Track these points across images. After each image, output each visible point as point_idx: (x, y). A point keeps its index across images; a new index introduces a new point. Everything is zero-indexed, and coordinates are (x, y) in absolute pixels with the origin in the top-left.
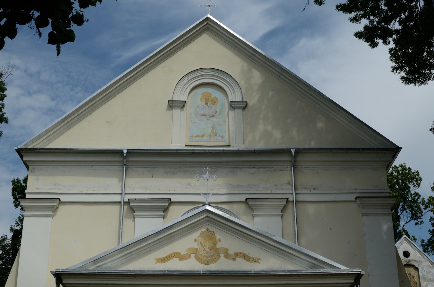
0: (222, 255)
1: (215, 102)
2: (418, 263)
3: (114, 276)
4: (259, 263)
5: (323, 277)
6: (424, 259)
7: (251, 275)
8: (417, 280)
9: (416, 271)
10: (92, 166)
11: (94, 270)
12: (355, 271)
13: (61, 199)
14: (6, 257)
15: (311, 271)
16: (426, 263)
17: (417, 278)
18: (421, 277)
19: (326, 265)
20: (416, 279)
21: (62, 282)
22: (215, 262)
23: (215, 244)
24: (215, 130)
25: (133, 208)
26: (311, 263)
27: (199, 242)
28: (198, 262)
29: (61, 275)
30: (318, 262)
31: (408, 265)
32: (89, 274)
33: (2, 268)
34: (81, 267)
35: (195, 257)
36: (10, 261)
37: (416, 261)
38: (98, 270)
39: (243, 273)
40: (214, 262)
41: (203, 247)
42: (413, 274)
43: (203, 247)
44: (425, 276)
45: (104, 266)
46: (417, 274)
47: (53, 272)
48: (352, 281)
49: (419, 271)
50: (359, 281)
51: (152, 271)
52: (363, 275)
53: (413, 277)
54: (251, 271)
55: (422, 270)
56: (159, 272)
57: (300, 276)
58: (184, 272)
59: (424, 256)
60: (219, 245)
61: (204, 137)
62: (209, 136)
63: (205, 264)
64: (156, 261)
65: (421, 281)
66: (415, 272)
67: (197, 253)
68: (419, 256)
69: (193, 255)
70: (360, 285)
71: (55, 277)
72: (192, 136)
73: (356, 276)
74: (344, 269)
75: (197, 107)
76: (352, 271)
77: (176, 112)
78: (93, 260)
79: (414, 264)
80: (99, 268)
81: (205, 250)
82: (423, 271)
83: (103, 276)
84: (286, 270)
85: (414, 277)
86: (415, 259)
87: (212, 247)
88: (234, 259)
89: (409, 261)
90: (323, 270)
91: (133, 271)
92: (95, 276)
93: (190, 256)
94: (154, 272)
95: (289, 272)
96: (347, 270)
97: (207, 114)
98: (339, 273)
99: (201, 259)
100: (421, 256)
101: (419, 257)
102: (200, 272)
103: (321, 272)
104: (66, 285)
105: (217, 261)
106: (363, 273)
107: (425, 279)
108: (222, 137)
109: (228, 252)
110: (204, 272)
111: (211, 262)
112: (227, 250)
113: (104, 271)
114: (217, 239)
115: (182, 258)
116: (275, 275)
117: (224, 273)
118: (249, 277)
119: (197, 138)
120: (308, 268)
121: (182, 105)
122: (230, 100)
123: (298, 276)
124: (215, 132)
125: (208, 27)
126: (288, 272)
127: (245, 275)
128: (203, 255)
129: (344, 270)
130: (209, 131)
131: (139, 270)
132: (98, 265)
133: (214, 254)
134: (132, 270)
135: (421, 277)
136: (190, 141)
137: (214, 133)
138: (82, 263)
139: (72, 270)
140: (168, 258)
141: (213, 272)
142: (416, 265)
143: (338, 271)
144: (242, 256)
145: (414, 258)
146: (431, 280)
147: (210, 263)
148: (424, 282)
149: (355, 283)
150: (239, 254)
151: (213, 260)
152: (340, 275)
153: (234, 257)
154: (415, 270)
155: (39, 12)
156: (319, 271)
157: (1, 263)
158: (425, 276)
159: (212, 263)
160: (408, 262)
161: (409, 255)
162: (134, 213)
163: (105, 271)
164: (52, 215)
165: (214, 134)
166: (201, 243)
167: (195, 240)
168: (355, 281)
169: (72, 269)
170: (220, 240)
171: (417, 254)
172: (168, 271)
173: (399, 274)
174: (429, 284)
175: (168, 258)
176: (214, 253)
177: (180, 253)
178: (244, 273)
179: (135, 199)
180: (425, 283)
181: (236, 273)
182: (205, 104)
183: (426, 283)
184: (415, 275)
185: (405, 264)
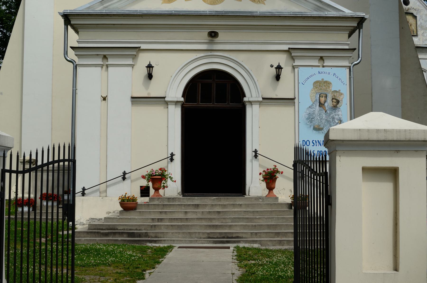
2: (416, 11)
3: (121, 16)
4: (265, 4)
5: (326, 19)
6: (423, 8)
7: (257, 16)
8: (415, 28)
9: (414, 20)
11: (102, 11)
12: (359, 14)
14: (10, 1)
15: (315, 13)
16: (425, 11)
17: (414, 26)
18: (419, 26)
19: (330, 8)
20: (413, 27)
21: (71, 22)
22: (221, 3)
26: (316, 5)
28: (204, 3)
29: (69, 16)
30: (323, 4)
31: (407, 13)
32: (97, 14)
33: (6, 13)
34: (89, 8)
36: (13, 5)
37: (415, 9)
38: (105, 11)
39: (248, 13)
40: (220, 2)
42: (411, 22)
44: (423, 24)
45: (111, 7)
46: (415, 22)
47: (61, 13)
48: (356, 25)
49: (417, 19)
50: (362, 24)
51: (158, 11)
52: (366, 19)
54: (257, 12)
55: (420, 18)
56: (166, 12)
57: (304, 18)
58: (190, 13)
59: (424, 5)
63: (211, 4)
65: (419, 29)
66: (413, 20)
68: (419, 5)
70: (362, 29)
71: (63, 18)
73: (359, 20)
74: (348, 12)
76: (356, 14)
78: (100, 1)
80: (107, 9)
82: (421, 20)
83: (111, 17)
84: (291, 12)
85: (411, 25)
86: (415, 7)
89: (408, 9)
90: (327, 13)
91: (140, 11)
92: (103, 16)
94: (161, 12)
95: (293, 14)
96: (351, 13)
98: (343, 17)
100: (420, 5)
102: (206, 13)
103: (325, 14)
104: (75, 26)
106: (366, 17)
107: (422, 27)
110: (210, 13)
111: (217, 3)
113: (111, 11)
116: (280, 16)
117: (230, 13)
118: (254, 18)
120: (312, 10)
123: (302, 18)
126: (292, 14)
127: (250, 16)
129: (348, 13)
131: (146, 11)
132: (105, 5)
134: (138, 10)
135: (419, 26)
138: (89, 3)
139: (80, 11)
141: (219, 13)
143: (342, 14)
145: (413, 6)
147: (216, 3)
148: (421, 30)
149: (357, 27)
152: (344, 19)
154: (413, 18)
156: (323, 13)
157: (6, 8)
158: (423, 25)
159: (218, 3)
160: (407, 10)
161: (409, 3)
163: (113, 11)
168: (358, 24)
169: (79, 9)
171: (417, 3)
172: (175, 11)
173: (399, 20)
174: (426, 33)
178: (250, 13)
180: (422, 31)
181: (243, 13)
183: (423, 32)
184: (413, 23)
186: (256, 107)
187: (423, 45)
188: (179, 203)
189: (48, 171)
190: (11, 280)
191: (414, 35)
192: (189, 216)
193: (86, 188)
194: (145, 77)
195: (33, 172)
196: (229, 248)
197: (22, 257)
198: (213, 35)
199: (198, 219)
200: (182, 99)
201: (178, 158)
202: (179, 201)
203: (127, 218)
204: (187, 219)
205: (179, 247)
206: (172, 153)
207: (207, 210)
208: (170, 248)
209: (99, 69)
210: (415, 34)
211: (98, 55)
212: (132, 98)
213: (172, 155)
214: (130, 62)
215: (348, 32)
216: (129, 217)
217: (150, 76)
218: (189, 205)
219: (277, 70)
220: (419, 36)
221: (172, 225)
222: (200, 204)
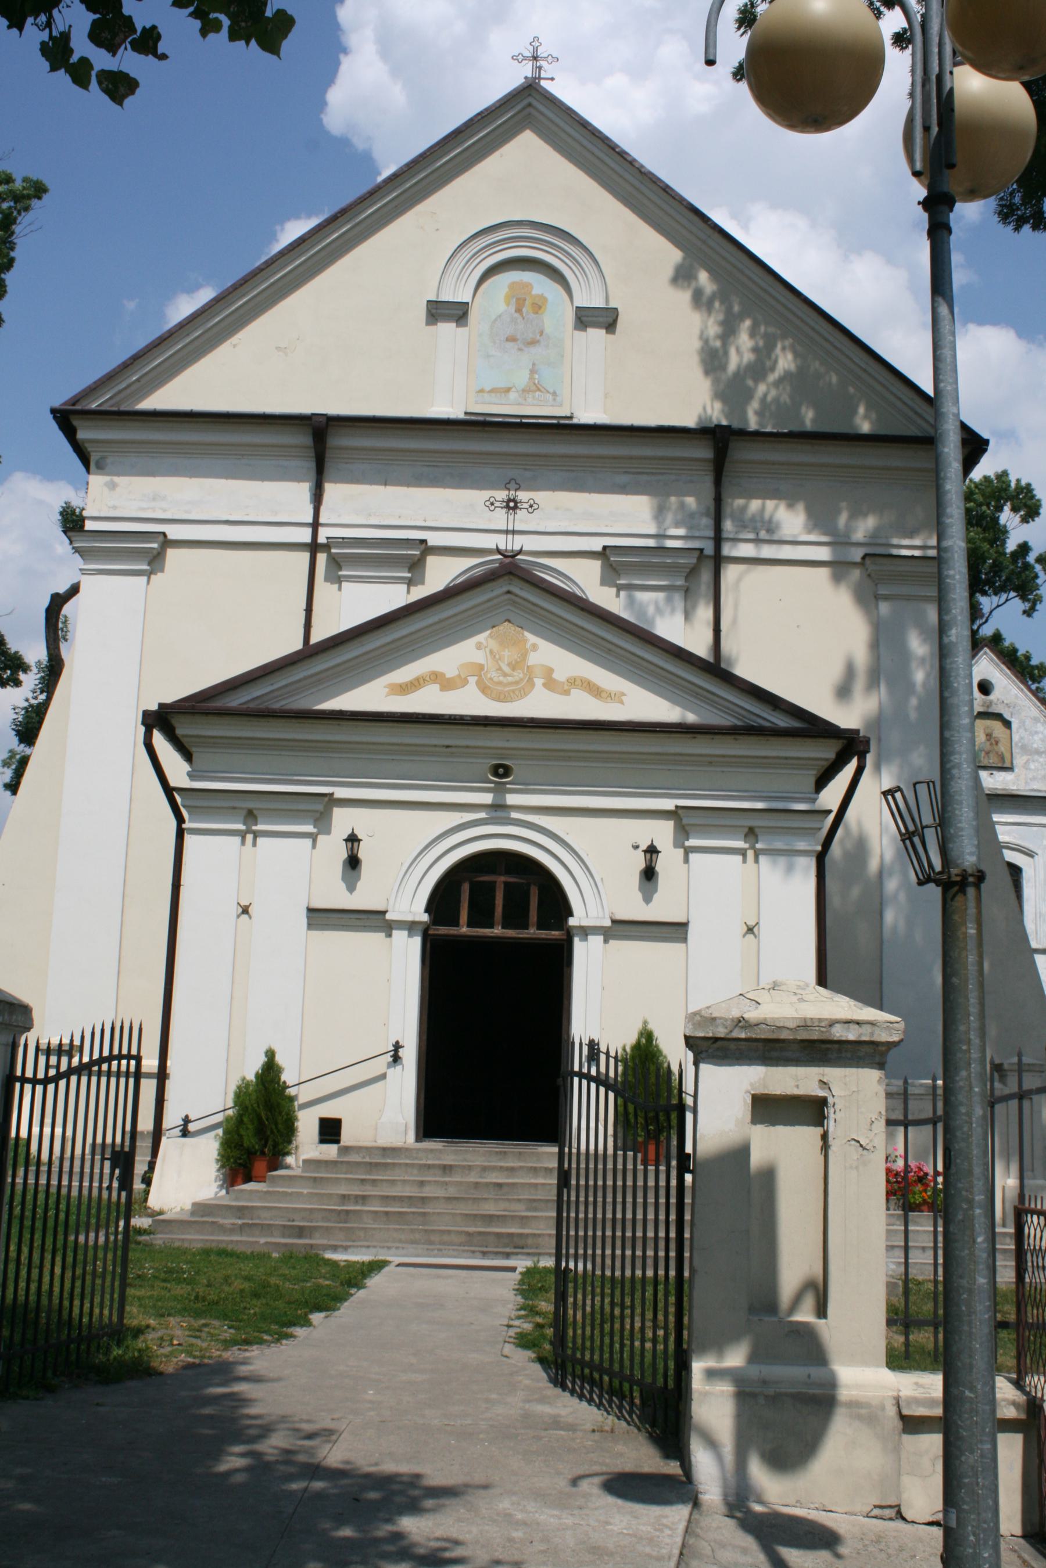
0: (539, 682)
1: (540, 307)
10: (243, 455)
13: (167, 534)
22: (522, 698)
23: (524, 656)
24: (537, 376)
25: (339, 560)
27: (487, 650)
35: (478, 683)
41: (497, 662)
43: (497, 662)
53: (997, 743)
60: (533, 659)
61: (511, 393)
62: (524, 391)
64: (387, 690)
67: (481, 676)
69: (473, 680)
72: (482, 391)
75: (496, 320)
77: (446, 328)
79: (1001, 712)
81: (500, 669)
82: (1021, 730)
83: (272, 684)
87: (517, 662)
88: (567, 693)
93: (465, 682)
97: (518, 337)
99: (490, 688)
101: (1016, 696)
105: (526, 695)
107: (1025, 749)
108: (554, 394)
114: (528, 646)
115: (447, 684)
119: (493, 395)
121: (458, 313)
122: (578, 303)
124: (536, 382)
125: (530, 114)
128: (496, 679)
130: (521, 378)
133: (522, 680)
136: (476, 403)
137: (535, 384)
140: (416, 684)
142: (1007, 716)
144: (585, 685)
146: (1038, 752)
150: (578, 682)
151: (517, 692)
153: (566, 687)
155: (342, 1264)
162: (340, 569)
164: (145, 571)
165: (534, 388)
166: (491, 652)
170: (535, 647)
174: (1033, 761)
175: (416, 684)
176: (521, 676)
177: (443, 675)
179: (343, 538)
180: (1025, 758)
182: (516, 311)
185: (981, 709)
186: (596, 941)
187: (1027, 791)
188: (408, 1161)
191: (1005, 766)
192: (428, 1191)
193: (192, 1117)
194: (344, 862)
196: (513, 1269)
199: (449, 1199)
200: (425, 918)
201: (410, 1054)
202: (407, 1157)
203: (292, 1192)
204: (423, 1199)
205: (399, 1265)
206: (397, 1042)
207: (473, 1178)
208: (376, 1266)
209: (237, 840)
210: (1007, 765)
211: (234, 808)
212: (311, 911)
213: (397, 1046)
215: (814, 772)
216: (289, 1190)
217: (353, 862)
218: (429, 1167)
219: (648, 855)
220: (1016, 770)
221: (387, 1213)
222: (456, 1166)
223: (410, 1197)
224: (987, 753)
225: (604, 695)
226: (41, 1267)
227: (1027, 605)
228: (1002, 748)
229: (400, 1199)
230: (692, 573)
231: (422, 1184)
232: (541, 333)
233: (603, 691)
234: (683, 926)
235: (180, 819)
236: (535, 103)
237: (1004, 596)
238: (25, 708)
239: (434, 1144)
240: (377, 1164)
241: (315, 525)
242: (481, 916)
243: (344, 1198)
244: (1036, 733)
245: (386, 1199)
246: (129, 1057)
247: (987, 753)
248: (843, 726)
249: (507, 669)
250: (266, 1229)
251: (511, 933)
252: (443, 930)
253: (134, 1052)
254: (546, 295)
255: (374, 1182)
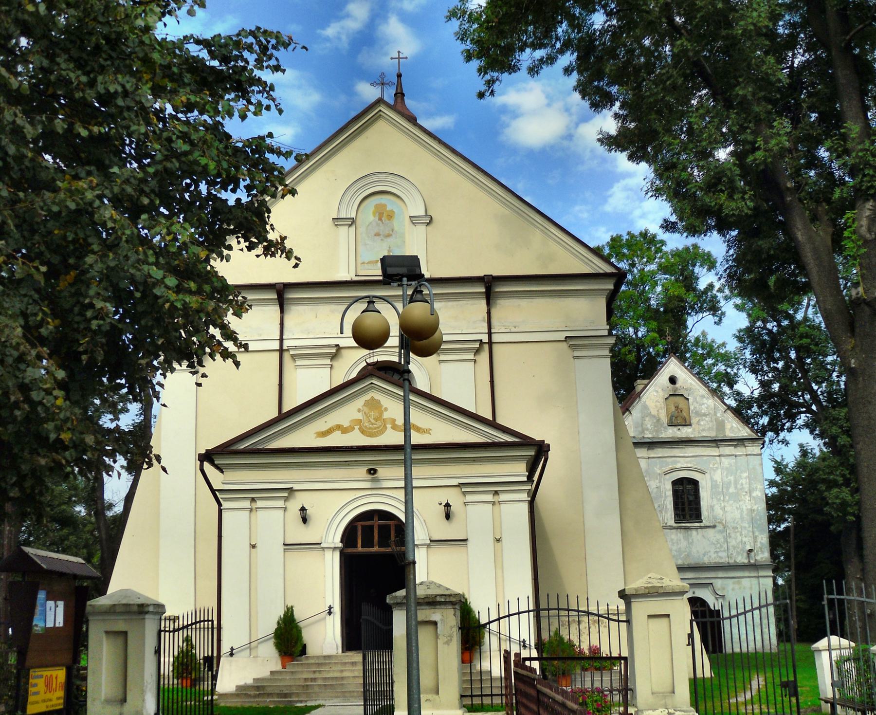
0: (389, 426)
15: (427, 475)
22: (381, 434)
23: (381, 414)
69: (357, 427)
77: (343, 230)
81: (370, 421)
93: (354, 429)
105: (383, 433)
107: (698, 414)
109: (396, 423)
112: (395, 420)
115: (345, 430)
133: (381, 426)
135: (692, 411)
166: (365, 413)
167: (359, 410)
180: (697, 419)
189: (192, 628)
190: (166, 712)
195: (440, 361)
197: (168, 711)
198: (372, 472)
200: (340, 545)
201: (337, 609)
214: (280, 503)
216: (280, 678)
217: (305, 520)
218: (346, 663)
223: (336, 677)
224: (676, 417)
225: (421, 431)
226: (182, 692)
227: (717, 319)
228: (685, 414)
229: (332, 678)
230: (477, 351)
231: (342, 671)
232: (393, 230)
233: (421, 428)
234: (466, 540)
235: (220, 504)
236: (382, 109)
237: (700, 315)
238: (133, 424)
239: (349, 653)
240: (322, 664)
241: (281, 340)
242: (368, 542)
243: (306, 679)
244: (703, 404)
245: (325, 679)
246: (208, 621)
247: (676, 417)
248: (537, 439)
249: (373, 421)
250: (270, 695)
251: (383, 550)
252: (350, 550)
253: (210, 619)
254: (394, 210)
255: (320, 672)
